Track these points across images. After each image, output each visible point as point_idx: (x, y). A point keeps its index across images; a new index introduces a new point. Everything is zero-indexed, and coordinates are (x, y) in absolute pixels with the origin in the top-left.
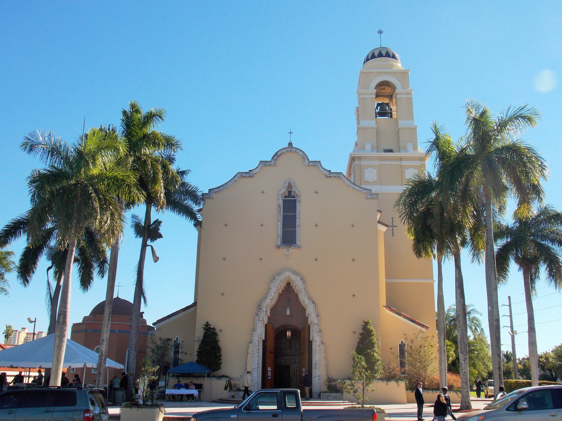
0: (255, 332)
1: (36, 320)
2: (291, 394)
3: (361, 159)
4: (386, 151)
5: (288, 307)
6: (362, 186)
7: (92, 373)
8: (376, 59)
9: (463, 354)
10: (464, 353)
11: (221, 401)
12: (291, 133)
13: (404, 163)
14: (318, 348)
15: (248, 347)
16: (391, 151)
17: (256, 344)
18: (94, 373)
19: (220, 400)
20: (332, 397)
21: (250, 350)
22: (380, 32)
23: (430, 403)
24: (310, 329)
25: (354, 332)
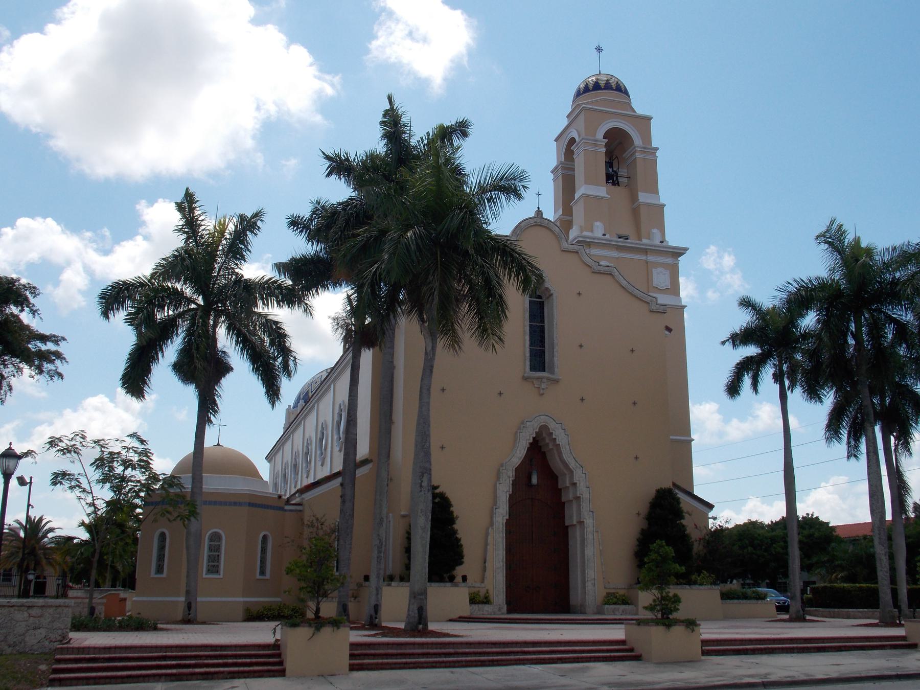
0: (497, 510)
1: (32, 481)
2: (733, 598)
3: (591, 246)
4: (620, 237)
5: (535, 472)
6: (650, 294)
7: (151, 576)
8: (620, 93)
9: (883, 546)
10: (885, 545)
11: (461, 619)
12: (538, 194)
13: (651, 258)
14: (590, 536)
15: (487, 534)
16: (626, 238)
17: (499, 528)
18: (207, 576)
19: (460, 617)
20: (621, 611)
21: (490, 538)
22: (599, 49)
23: (766, 618)
24: (4, 517)
25: (638, 514)
